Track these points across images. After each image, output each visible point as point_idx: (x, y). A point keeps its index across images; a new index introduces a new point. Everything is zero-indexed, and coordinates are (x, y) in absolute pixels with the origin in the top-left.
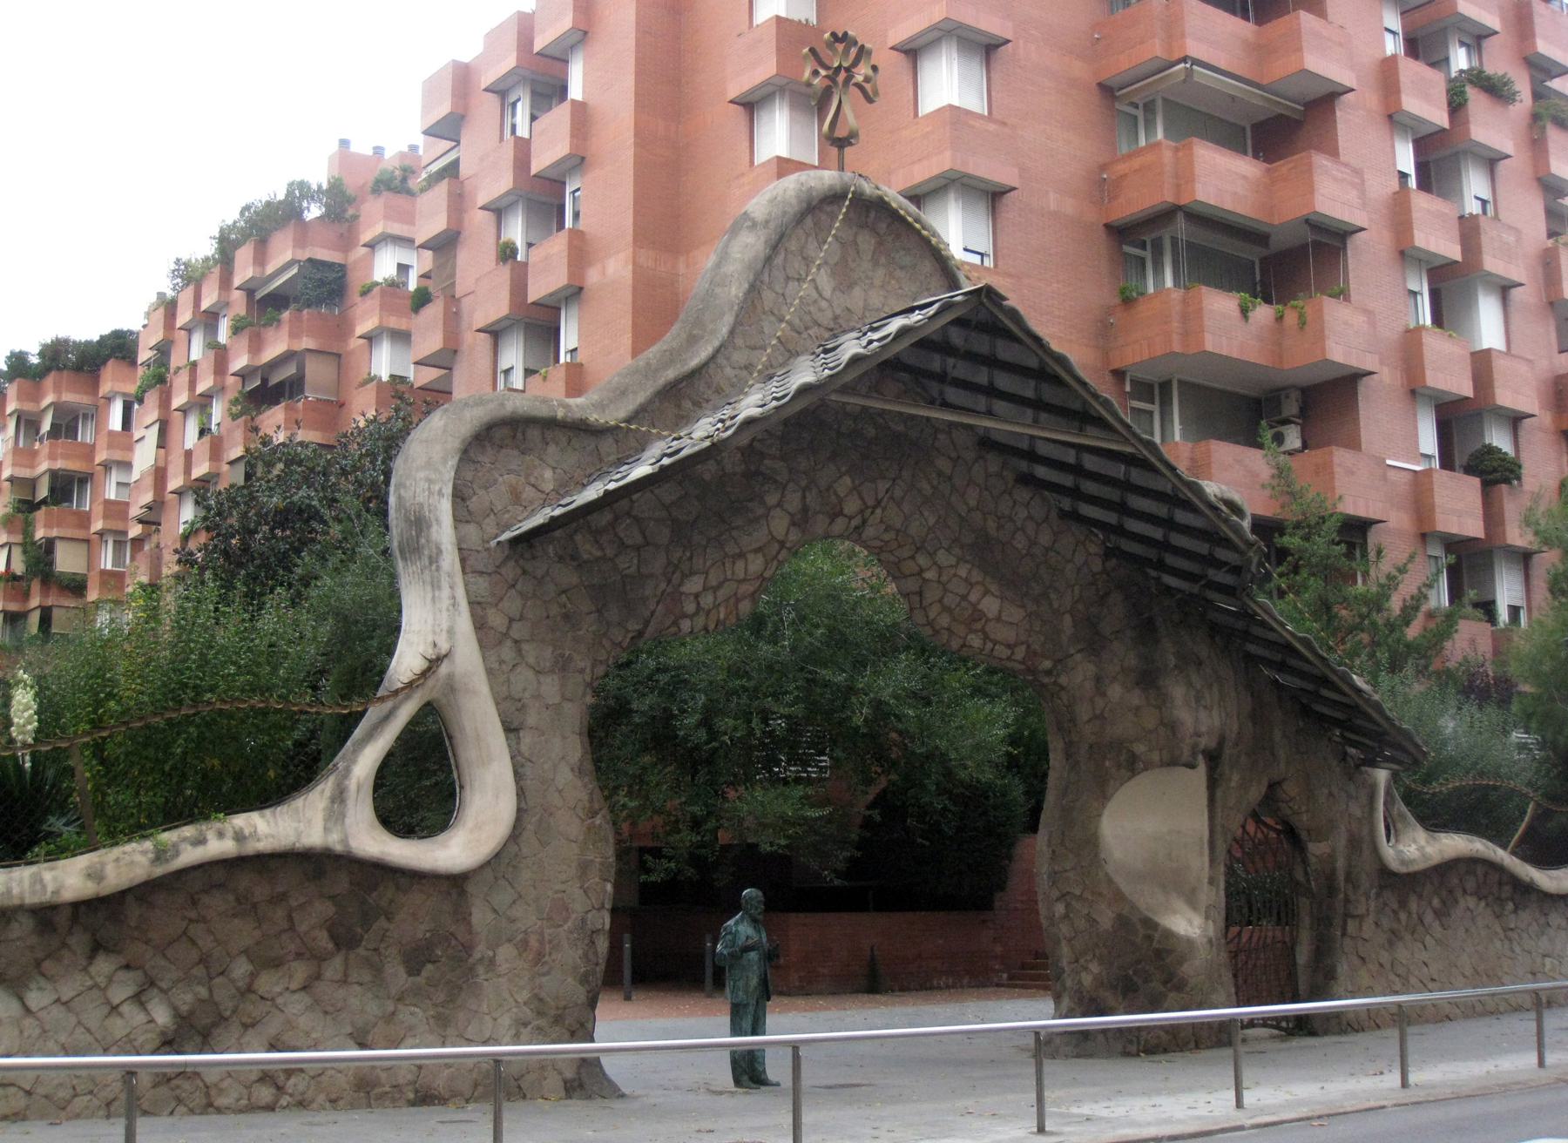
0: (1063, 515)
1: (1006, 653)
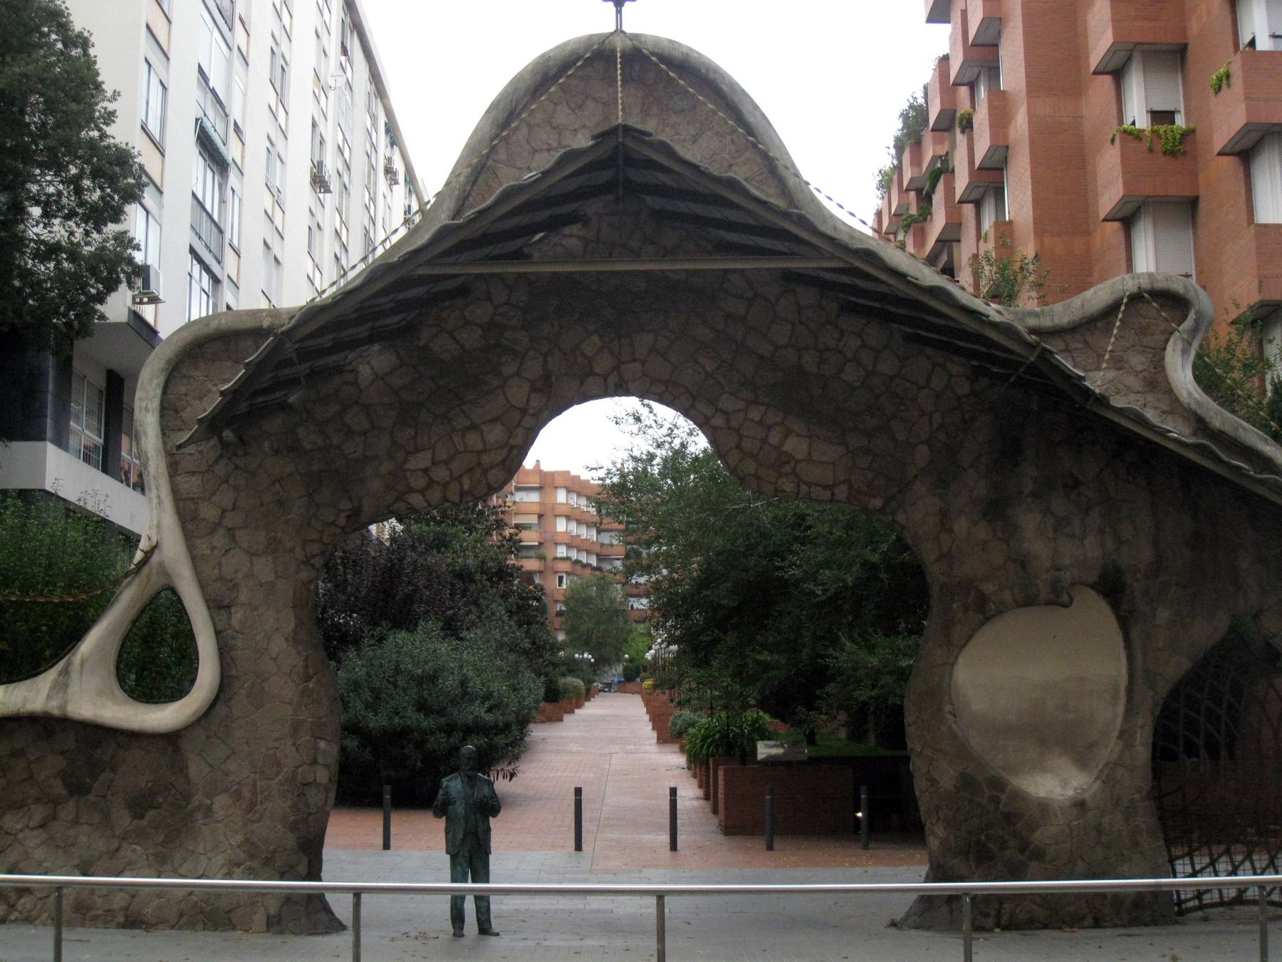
0: (909, 338)
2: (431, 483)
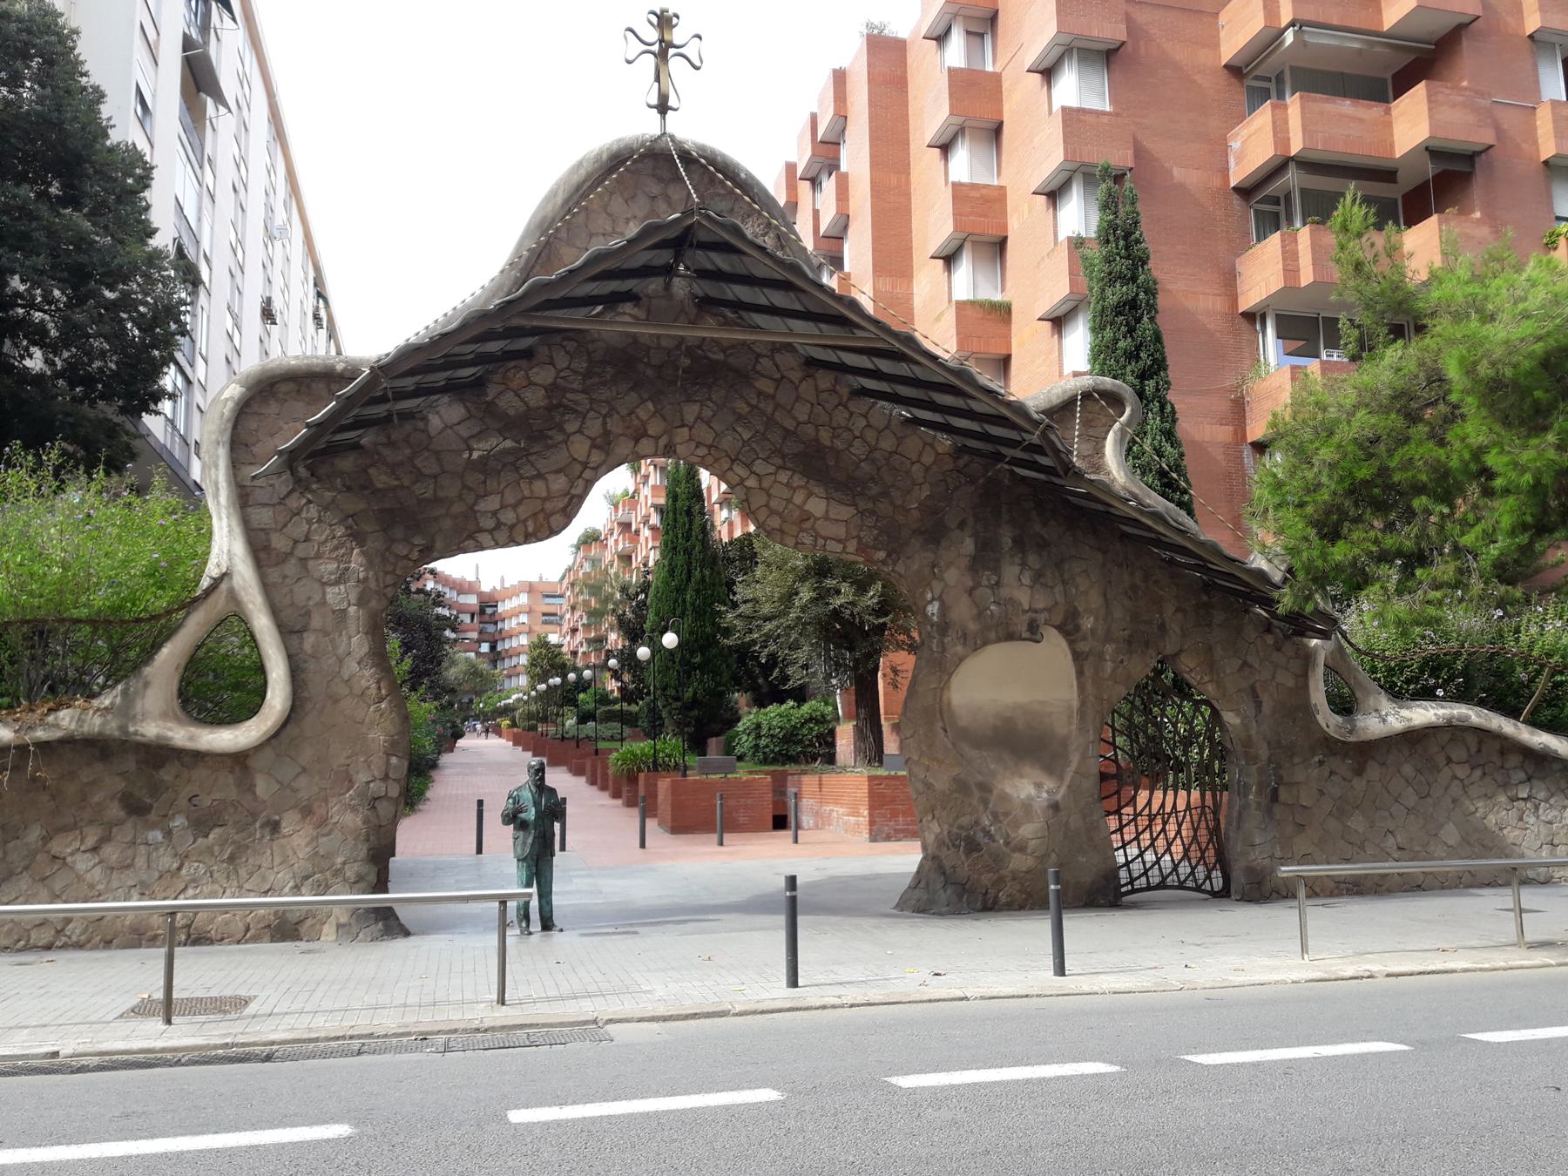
1: (839, 548)
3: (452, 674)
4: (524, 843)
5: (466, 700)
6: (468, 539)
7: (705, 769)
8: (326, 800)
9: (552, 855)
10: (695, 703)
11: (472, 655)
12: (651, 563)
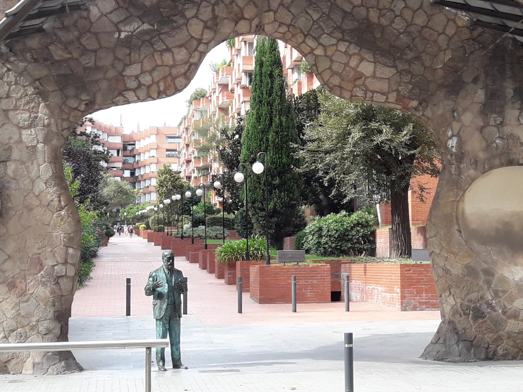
2: (140, 85)
3: (106, 192)
4: (161, 308)
5: (115, 210)
6: (118, 95)
7: (283, 259)
8: (25, 279)
9: (180, 317)
10: (275, 212)
11: (118, 179)
12: (243, 113)
